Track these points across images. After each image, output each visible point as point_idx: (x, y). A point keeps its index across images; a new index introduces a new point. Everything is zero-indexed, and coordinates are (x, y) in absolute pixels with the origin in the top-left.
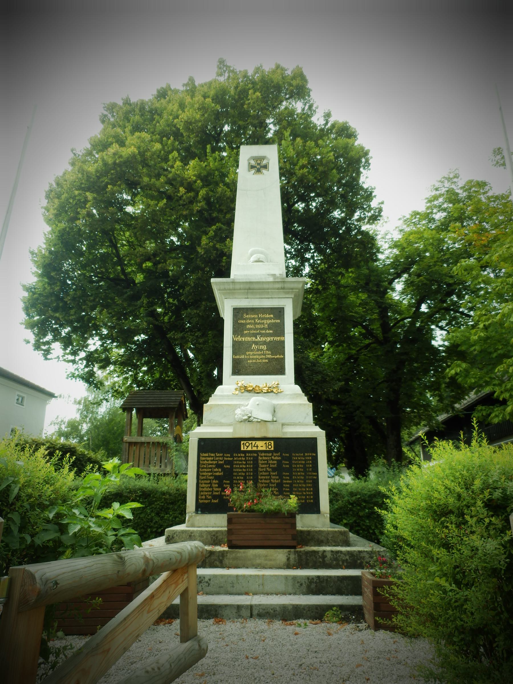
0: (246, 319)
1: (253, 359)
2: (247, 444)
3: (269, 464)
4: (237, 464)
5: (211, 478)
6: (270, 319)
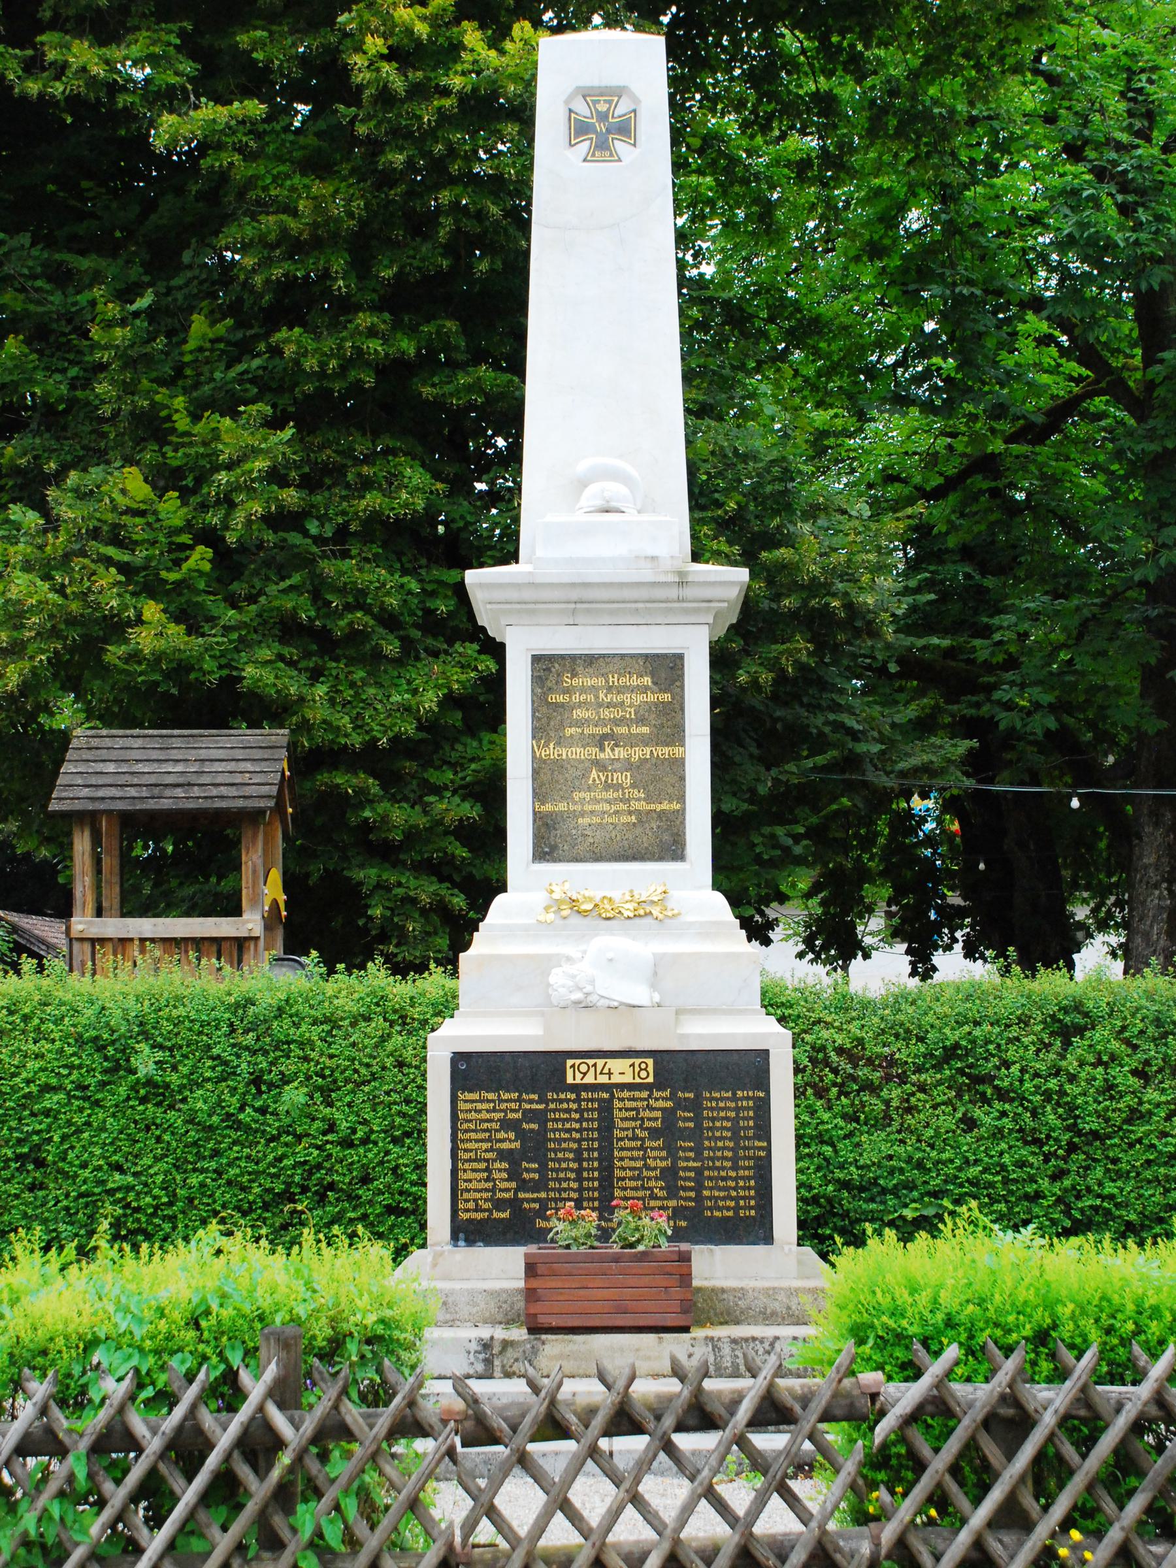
4: (556, 1120)
5: (489, 1155)
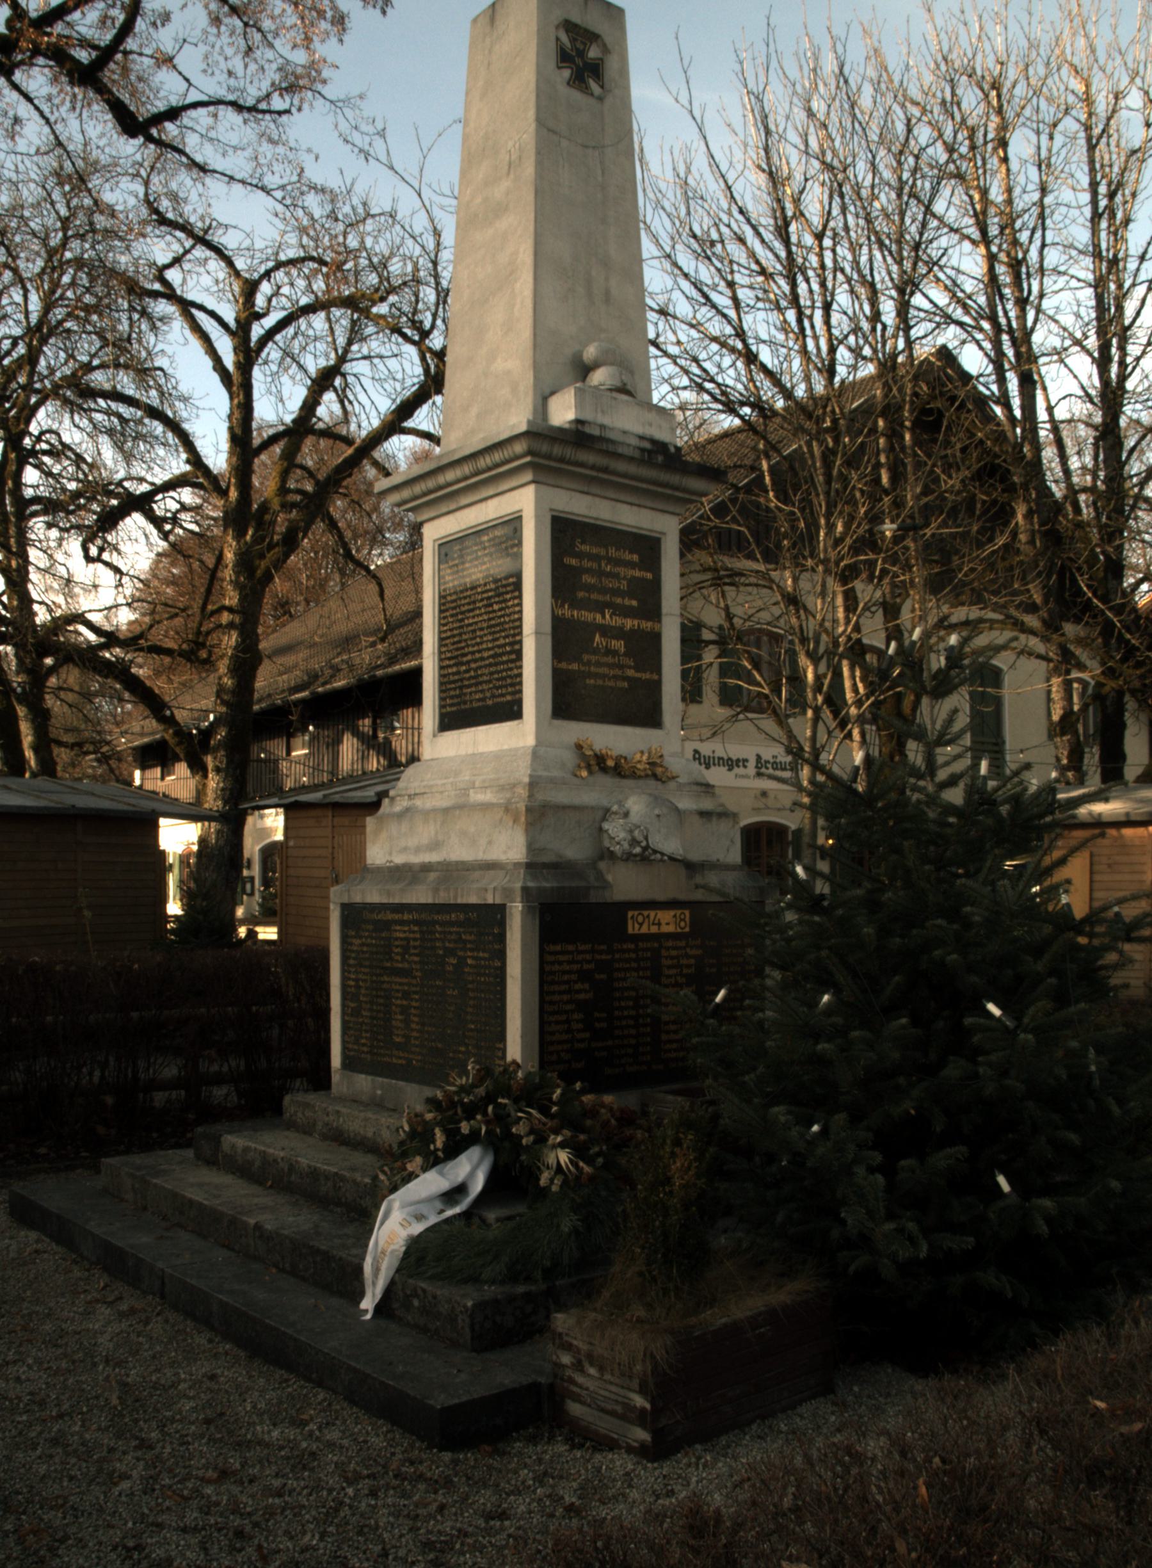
0: (580, 556)
1: (596, 676)
2: (640, 919)
5: (569, 1007)
6: (631, 565)
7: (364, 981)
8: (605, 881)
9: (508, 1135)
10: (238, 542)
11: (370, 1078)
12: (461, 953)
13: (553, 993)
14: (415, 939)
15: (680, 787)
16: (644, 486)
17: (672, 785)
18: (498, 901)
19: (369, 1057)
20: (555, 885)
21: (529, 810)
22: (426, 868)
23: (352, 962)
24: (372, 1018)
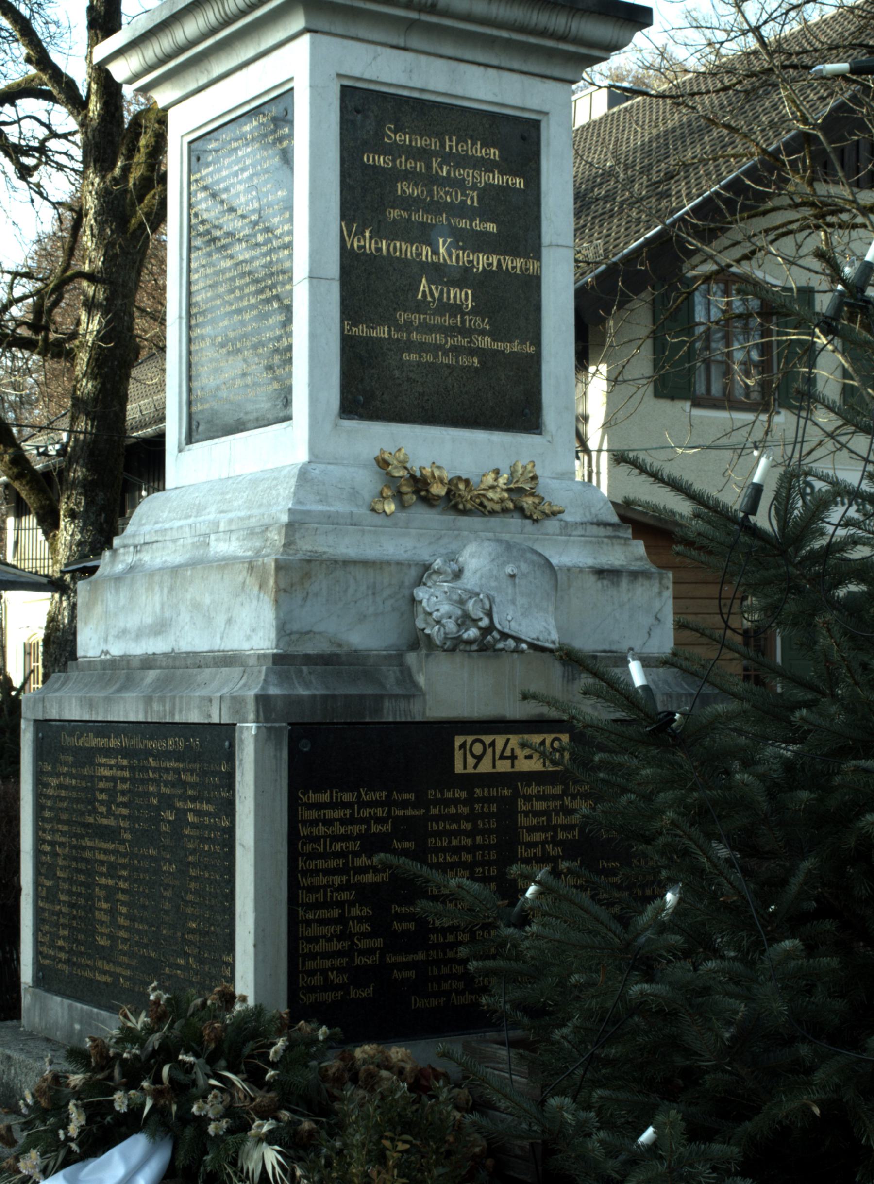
1: (422, 347)
3: (554, 829)
4: (439, 834)
5: (344, 896)
6: (488, 165)
7: (62, 845)
8: (415, 685)
9: (186, 1118)
10: (103, 178)
11: (67, 1002)
12: (180, 804)
13: (316, 872)
14: (124, 780)
15: (567, 528)
16: (505, 34)
17: (551, 525)
18: (225, 720)
19: (65, 968)
20: (320, 691)
21: (280, 567)
22: (148, 662)
23: (47, 814)
24: (72, 906)
